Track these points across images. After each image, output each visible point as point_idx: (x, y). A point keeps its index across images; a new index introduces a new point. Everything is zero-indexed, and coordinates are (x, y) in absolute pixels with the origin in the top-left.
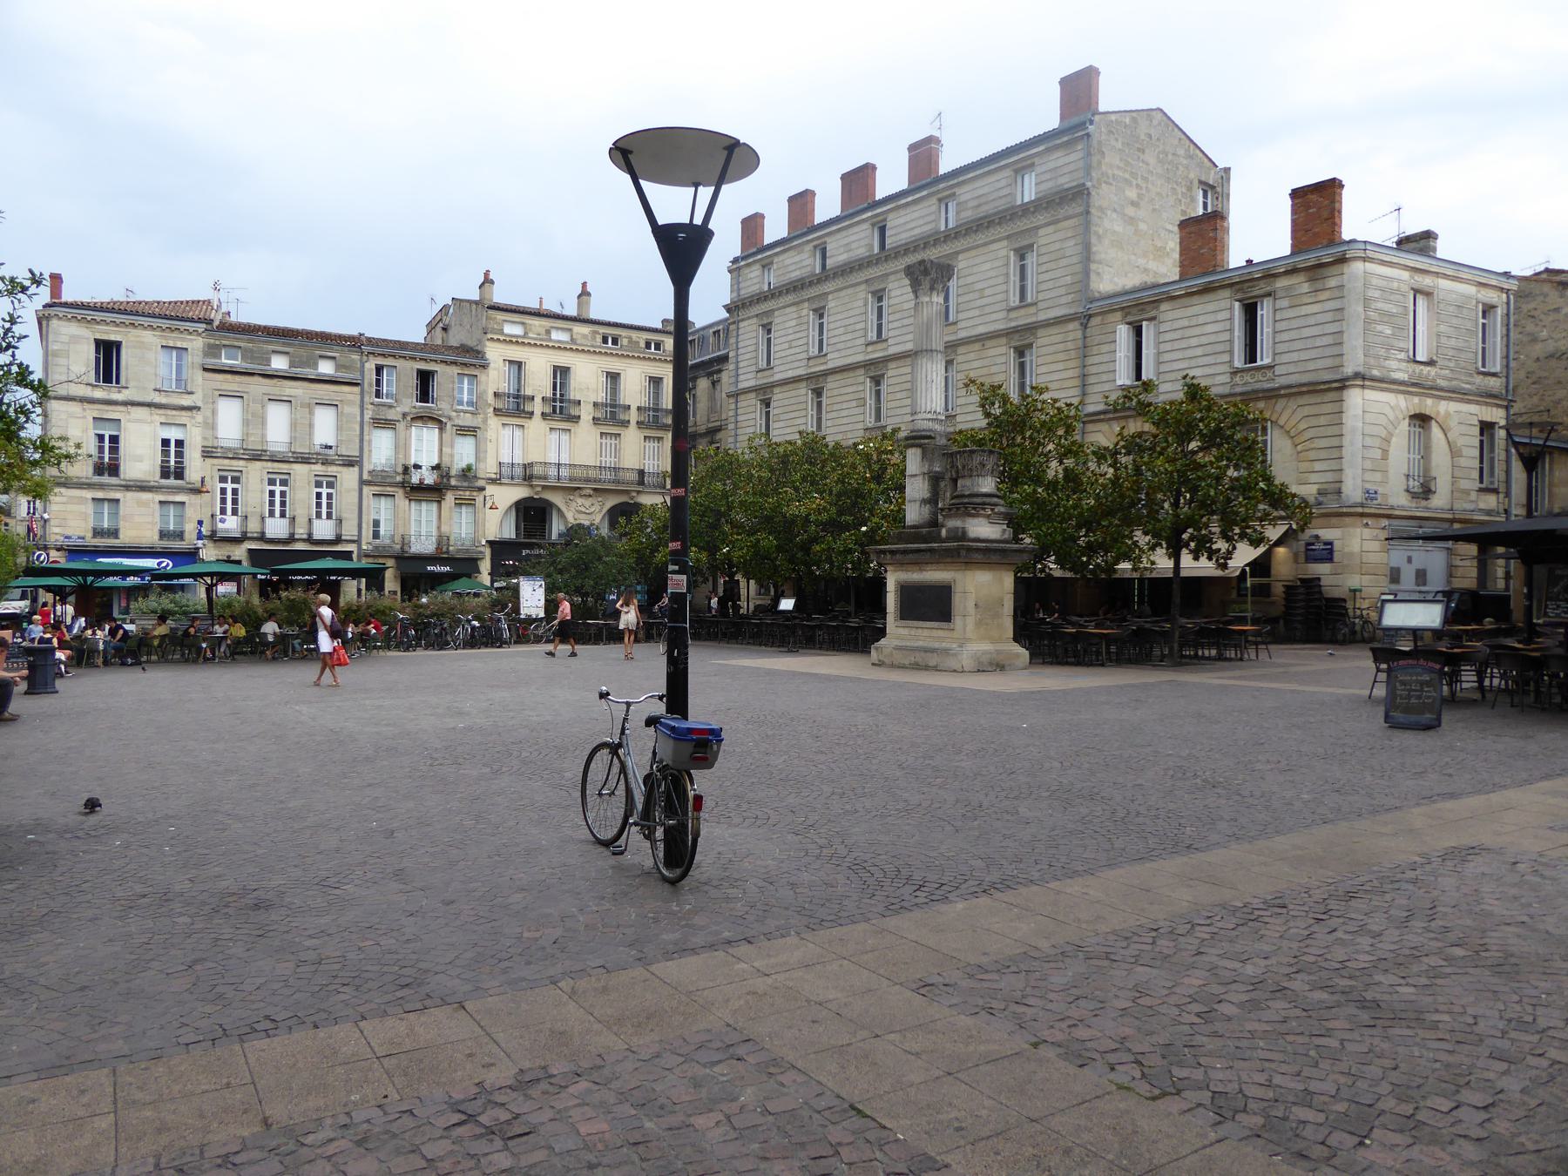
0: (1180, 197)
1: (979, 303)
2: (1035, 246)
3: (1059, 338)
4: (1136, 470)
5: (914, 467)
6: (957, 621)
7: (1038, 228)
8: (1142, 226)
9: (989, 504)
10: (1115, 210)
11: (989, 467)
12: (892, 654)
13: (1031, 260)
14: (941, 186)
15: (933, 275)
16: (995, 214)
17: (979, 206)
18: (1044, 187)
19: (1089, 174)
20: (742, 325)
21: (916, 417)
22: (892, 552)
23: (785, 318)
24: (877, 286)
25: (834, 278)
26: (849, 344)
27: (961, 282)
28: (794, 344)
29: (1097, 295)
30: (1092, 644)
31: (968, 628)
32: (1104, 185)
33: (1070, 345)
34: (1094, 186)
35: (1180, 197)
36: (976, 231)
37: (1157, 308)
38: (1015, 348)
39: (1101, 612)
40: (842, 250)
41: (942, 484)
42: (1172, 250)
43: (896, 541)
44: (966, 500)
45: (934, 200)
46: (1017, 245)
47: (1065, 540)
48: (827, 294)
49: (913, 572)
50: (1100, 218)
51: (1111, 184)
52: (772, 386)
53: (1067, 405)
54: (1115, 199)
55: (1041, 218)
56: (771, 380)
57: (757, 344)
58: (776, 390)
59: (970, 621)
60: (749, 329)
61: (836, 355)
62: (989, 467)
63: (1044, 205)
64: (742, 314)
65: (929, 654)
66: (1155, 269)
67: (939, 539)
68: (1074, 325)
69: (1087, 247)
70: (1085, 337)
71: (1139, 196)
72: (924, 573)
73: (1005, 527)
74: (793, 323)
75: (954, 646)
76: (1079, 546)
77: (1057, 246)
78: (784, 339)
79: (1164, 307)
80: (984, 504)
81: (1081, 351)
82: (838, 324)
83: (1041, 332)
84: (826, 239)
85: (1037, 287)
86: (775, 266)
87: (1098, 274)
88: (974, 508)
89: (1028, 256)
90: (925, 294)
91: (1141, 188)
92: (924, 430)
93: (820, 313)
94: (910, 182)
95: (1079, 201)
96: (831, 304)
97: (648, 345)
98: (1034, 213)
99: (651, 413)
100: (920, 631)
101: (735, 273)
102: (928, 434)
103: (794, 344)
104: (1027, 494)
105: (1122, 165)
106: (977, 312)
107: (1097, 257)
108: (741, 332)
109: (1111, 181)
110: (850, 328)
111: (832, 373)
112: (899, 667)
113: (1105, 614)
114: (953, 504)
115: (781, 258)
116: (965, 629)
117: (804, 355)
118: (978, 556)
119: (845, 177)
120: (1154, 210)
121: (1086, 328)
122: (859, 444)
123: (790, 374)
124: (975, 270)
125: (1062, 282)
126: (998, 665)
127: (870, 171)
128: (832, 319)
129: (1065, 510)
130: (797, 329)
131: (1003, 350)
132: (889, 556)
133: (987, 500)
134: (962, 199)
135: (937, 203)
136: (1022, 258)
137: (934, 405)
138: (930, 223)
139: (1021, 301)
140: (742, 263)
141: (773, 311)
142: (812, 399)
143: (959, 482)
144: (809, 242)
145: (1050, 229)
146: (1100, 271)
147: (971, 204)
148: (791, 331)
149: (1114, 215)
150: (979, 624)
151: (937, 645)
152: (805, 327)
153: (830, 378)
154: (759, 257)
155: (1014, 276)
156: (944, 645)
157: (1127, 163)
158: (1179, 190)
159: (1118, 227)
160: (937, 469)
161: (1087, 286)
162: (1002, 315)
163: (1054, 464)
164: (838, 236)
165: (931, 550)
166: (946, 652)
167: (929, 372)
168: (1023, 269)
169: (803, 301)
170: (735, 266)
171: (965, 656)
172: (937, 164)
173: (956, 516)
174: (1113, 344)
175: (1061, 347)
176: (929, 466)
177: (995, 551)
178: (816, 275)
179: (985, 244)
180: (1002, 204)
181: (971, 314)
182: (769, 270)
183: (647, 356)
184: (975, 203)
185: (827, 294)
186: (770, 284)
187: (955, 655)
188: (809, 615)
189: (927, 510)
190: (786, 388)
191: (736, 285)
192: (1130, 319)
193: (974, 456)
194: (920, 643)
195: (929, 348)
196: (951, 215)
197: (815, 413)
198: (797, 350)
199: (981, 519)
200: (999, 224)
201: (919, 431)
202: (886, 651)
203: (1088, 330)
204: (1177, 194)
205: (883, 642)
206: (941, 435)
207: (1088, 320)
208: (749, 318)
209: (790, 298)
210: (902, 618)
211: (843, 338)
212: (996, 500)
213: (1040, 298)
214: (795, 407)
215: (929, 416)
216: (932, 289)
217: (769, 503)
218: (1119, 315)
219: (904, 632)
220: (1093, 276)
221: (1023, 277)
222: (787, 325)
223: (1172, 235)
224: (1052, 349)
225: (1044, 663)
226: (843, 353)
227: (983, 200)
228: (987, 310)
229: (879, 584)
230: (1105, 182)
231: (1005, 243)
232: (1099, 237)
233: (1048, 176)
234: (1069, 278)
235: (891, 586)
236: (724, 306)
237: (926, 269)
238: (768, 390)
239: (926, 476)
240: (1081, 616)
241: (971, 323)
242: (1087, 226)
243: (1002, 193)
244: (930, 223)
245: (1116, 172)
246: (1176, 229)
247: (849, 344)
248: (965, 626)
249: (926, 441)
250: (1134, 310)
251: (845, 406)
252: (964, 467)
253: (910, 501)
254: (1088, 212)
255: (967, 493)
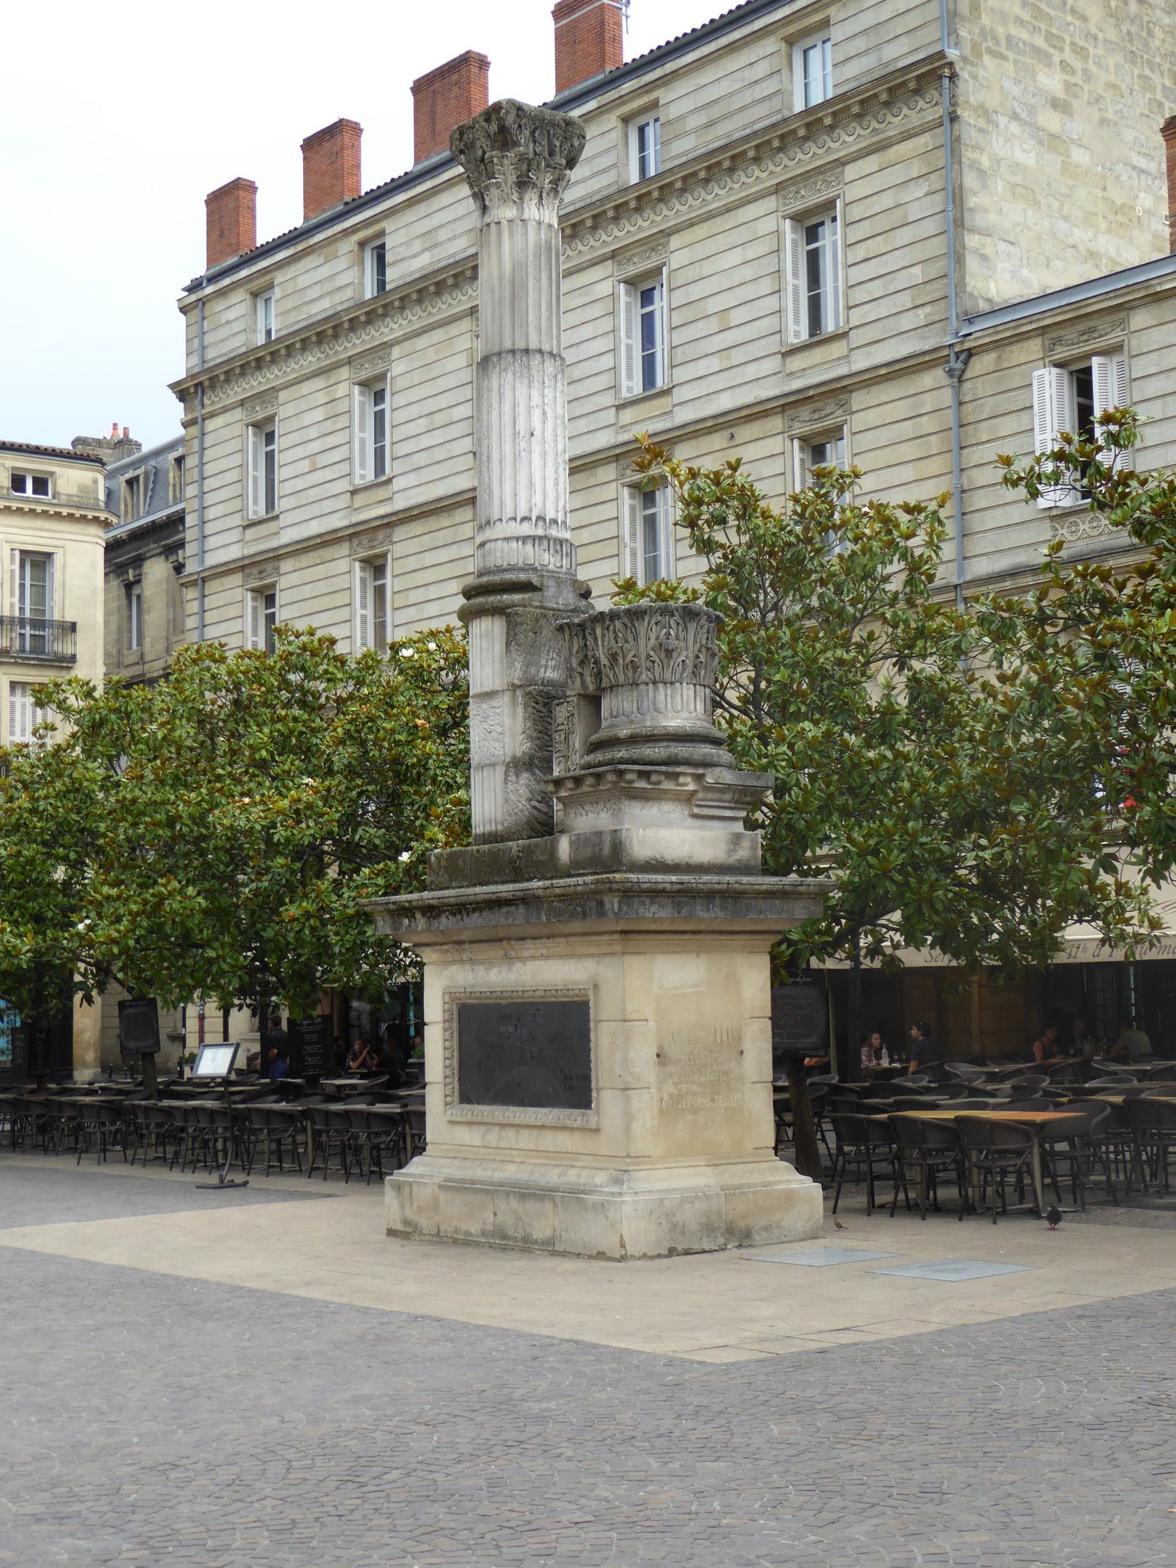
0: (1159, 96)
1: (719, 342)
2: (839, 204)
3: (901, 409)
4: (1097, 657)
5: (488, 670)
6: (607, 1100)
7: (841, 163)
8: (1079, 156)
9: (688, 763)
10: (1015, 116)
11: (685, 656)
12: (435, 1203)
13: (831, 239)
14: (628, 86)
15: (525, 146)
16: (746, 139)
17: (711, 124)
18: (851, 70)
19: (952, 31)
20: (210, 425)
21: (489, 534)
22: (431, 911)
23: (303, 405)
24: (812, 198)
25: (402, 308)
26: (439, 454)
27: (679, 298)
28: (322, 460)
29: (983, 306)
30: (1003, 1153)
31: (636, 1127)
32: (987, 59)
33: (927, 424)
34: (964, 59)
35: (1159, 96)
36: (707, 181)
37: (1123, 324)
38: (803, 439)
39: (1037, 1048)
40: (418, 246)
41: (561, 713)
42: (1149, 213)
43: (443, 879)
44: (622, 753)
45: (611, 121)
46: (798, 206)
47: (915, 864)
48: (387, 346)
49: (489, 963)
50: (981, 130)
51: (1005, 58)
52: (276, 556)
53: (908, 509)
54: (1016, 91)
55: (849, 140)
56: (275, 543)
57: (243, 466)
58: (286, 565)
59: (645, 1104)
60: (226, 433)
61: (411, 480)
62: (685, 656)
63: (856, 109)
64: (213, 402)
65: (532, 1206)
66: (1112, 252)
67: (549, 867)
68: (936, 377)
69: (956, 196)
70: (961, 404)
71: (1068, 86)
72: (518, 966)
73: (739, 827)
74: (319, 414)
75: (600, 1178)
76: (959, 882)
77: (887, 200)
78: (300, 452)
79: (1138, 319)
80: (673, 761)
81: (952, 434)
82: (414, 411)
83: (858, 400)
84: (386, 225)
85: (846, 295)
86: (277, 293)
87: (984, 258)
88: (641, 774)
89: (826, 231)
90: (504, 200)
91: (1073, 72)
92: (512, 568)
93: (375, 387)
94: (560, 87)
95: (933, 94)
96: (399, 367)
97: (18, 483)
98: (832, 127)
99: (28, 631)
100: (511, 1133)
101: (196, 313)
102: (523, 577)
103: (322, 460)
104: (811, 745)
105: (1026, 16)
106: (714, 364)
107: (979, 220)
108: (209, 440)
109: (1003, 49)
110: (439, 419)
111: (402, 522)
112: (455, 1242)
113: (1047, 1054)
114: (588, 766)
115: (290, 272)
116: (628, 1131)
117: (343, 486)
118: (659, 914)
119: (422, 88)
120: (1104, 122)
121: (961, 381)
122: (403, 645)
123: (314, 528)
124: (707, 268)
125: (903, 280)
126: (730, 1231)
127: (475, 70)
128: (400, 400)
129: (915, 786)
130: (327, 427)
131: (776, 444)
132: (421, 922)
133: (682, 750)
134: (674, 111)
135: (619, 124)
136: (812, 234)
137: (537, 499)
138: (605, 171)
139: (812, 335)
140: (209, 290)
141: (275, 390)
142: (363, 581)
143: (605, 703)
144: (347, 233)
145: (871, 163)
146: (988, 251)
147: (693, 122)
148: (313, 433)
149: (1015, 128)
150: (671, 1110)
151: (552, 1176)
152: (343, 422)
153: (400, 533)
154: (244, 273)
155: (796, 275)
156: (573, 1176)
157: (1039, 14)
158: (1156, 79)
159: (1024, 153)
160: (551, 674)
161: (961, 285)
162: (344, 500)
163: (885, 670)
164: (410, 215)
165: (526, 900)
166: (575, 1196)
167: (522, 409)
168: (814, 259)
169: (336, 366)
170: (193, 298)
171: (627, 1210)
172: (617, 41)
173: (595, 799)
174: (1024, 416)
175: (908, 428)
176: (528, 666)
177: (710, 895)
178: (364, 303)
179: (728, 209)
180: (760, 117)
181: (701, 368)
182: (267, 301)
183: (14, 505)
184: (702, 119)
185: (387, 346)
186: (268, 333)
187: (601, 1207)
188: (313, 1081)
189: (523, 786)
190: (305, 560)
191: (196, 341)
192: (1062, 353)
193: (642, 626)
194: (510, 1172)
195: (521, 345)
196: (273, 319)
197: (370, 612)
198: (328, 474)
199: (667, 807)
200: (757, 160)
201: (500, 570)
202: (424, 1194)
203: (967, 386)
204: (1153, 89)
205: (416, 1167)
206: (559, 581)
207: (966, 363)
208: (225, 410)
209: (311, 360)
210: (466, 1097)
211: (426, 441)
212: (706, 750)
213: (854, 322)
214: (326, 602)
215: (526, 529)
216: (523, 184)
217: (187, 803)
218: (1034, 347)
219: (470, 1137)
220: (972, 263)
221: (814, 278)
222: (309, 418)
223: (1145, 181)
224: (885, 435)
225: (872, 1208)
226: (427, 475)
227: (717, 111)
228: (737, 356)
229: (412, 995)
230: (991, 52)
231: (770, 203)
232: (982, 173)
233: (860, 44)
234: (917, 270)
235: (434, 1008)
236: (172, 386)
237: (503, 129)
238: (269, 567)
239: (519, 693)
240: (979, 1061)
241: (700, 389)
242: (954, 146)
243: (760, 92)
244: (605, 171)
245: (1014, 31)
246: (1160, 139)
247: (439, 454)
248: (628, 1117)
249: (517, 597)
250: (1070, 334)
251: (433, 592)
252: (614, 657)
253: (477, 768)
254: (954, 118)
255: (624, 733)
